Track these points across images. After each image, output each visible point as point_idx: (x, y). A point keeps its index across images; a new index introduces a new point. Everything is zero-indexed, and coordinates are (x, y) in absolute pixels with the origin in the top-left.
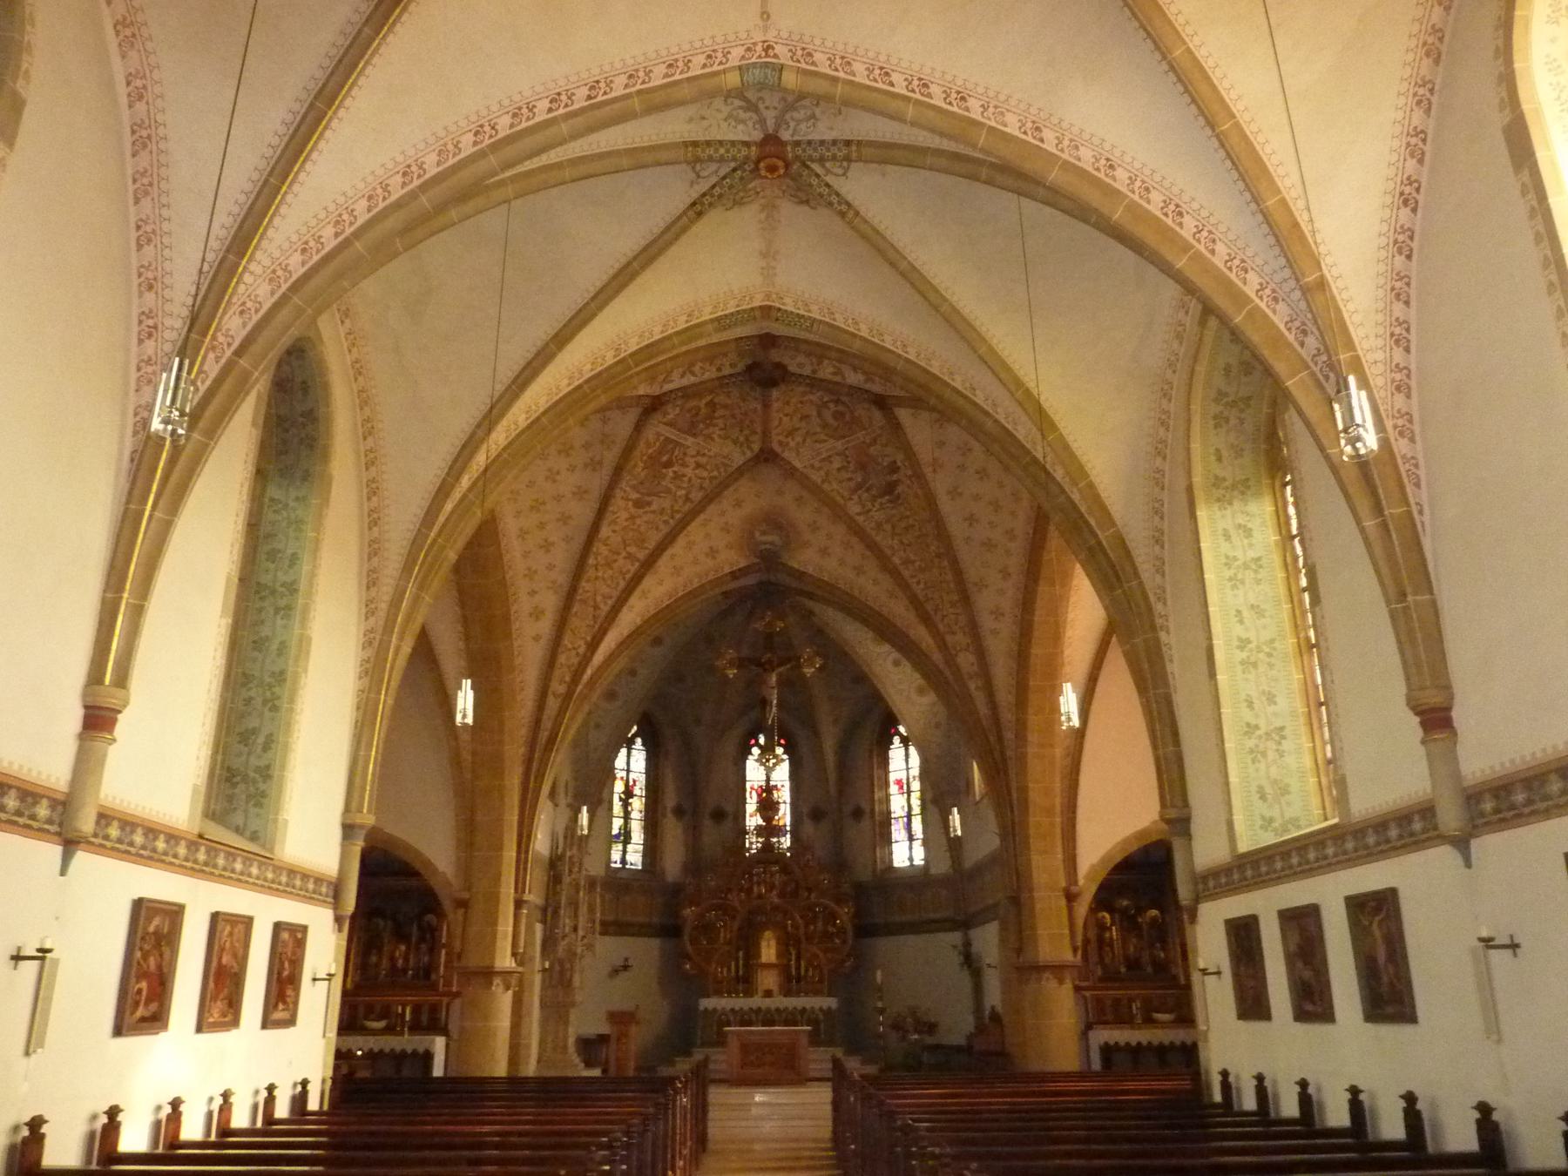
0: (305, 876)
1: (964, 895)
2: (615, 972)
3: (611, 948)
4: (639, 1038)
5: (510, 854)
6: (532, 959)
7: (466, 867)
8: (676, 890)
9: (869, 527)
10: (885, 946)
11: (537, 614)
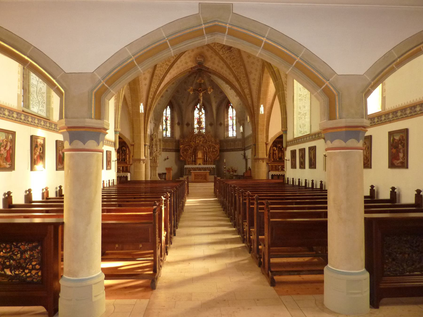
0: (110, 142)
1: (241, 144)
2: (165, 159)
3: (165, 154)
4: (172, 173)
5: (142, 134)
6: (148, 157)
7: (133, 138)
8: (179, 141)
9: (224, 58)
10: (226, 154)
11: (145, 79)
